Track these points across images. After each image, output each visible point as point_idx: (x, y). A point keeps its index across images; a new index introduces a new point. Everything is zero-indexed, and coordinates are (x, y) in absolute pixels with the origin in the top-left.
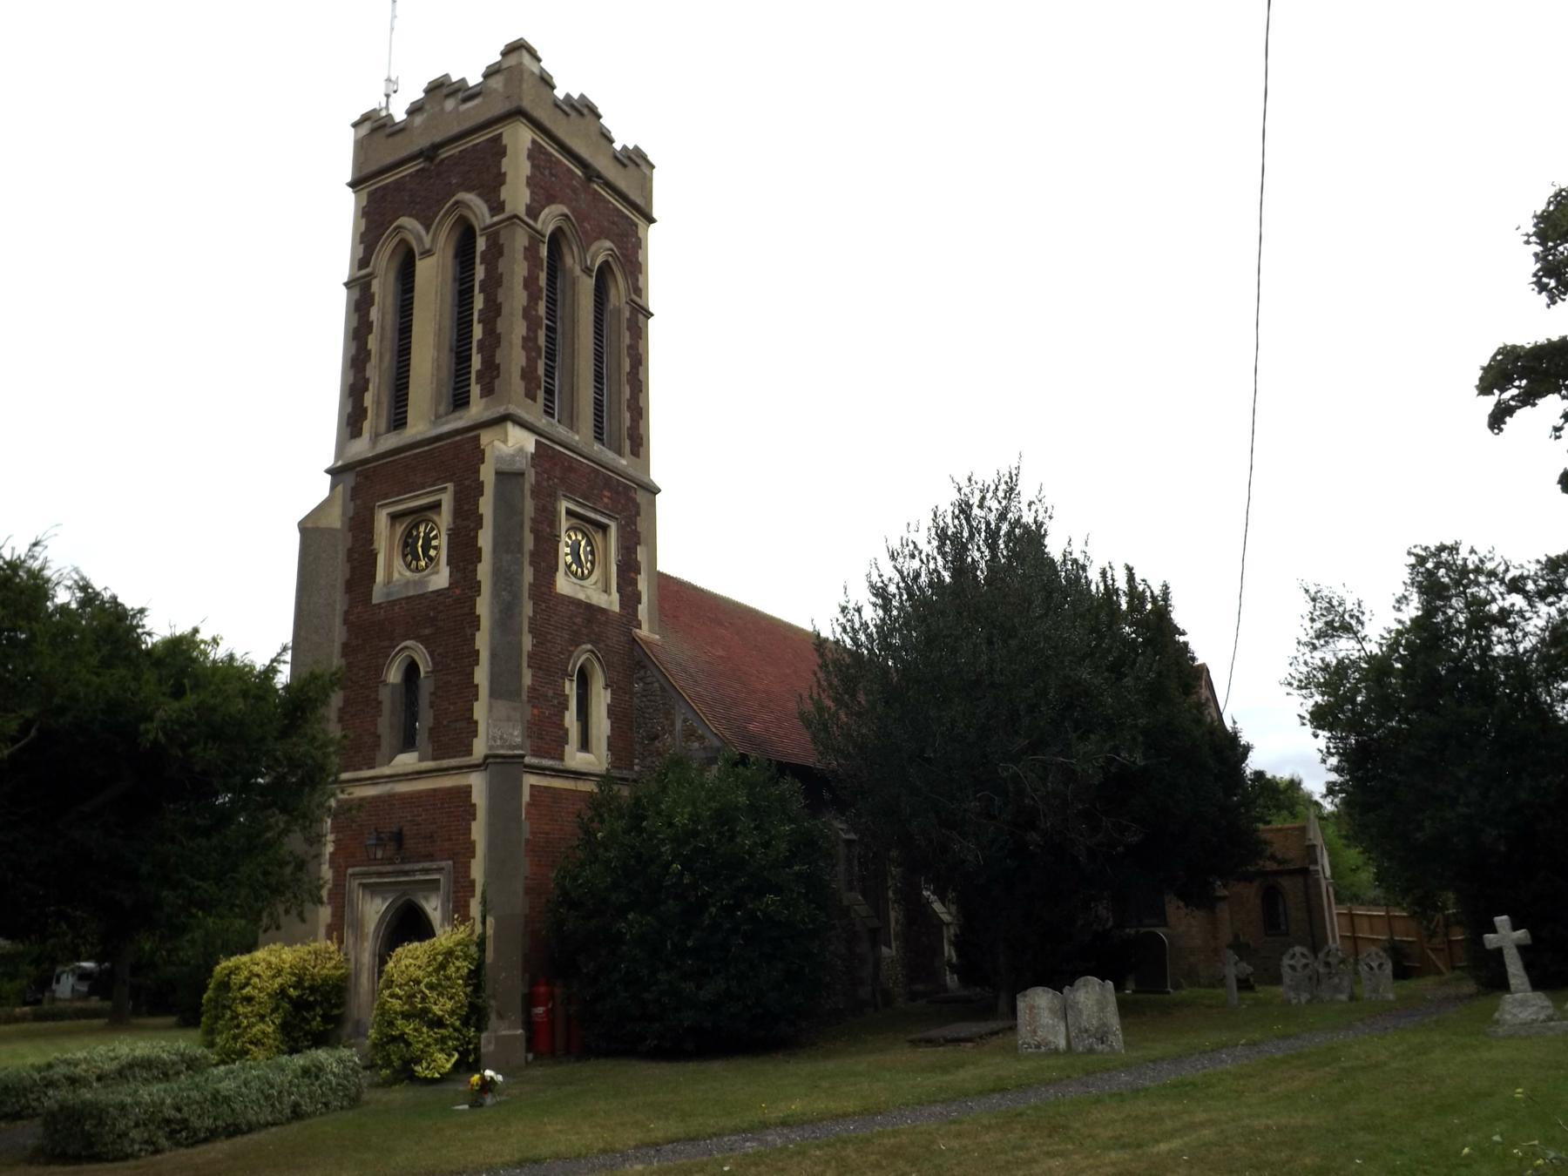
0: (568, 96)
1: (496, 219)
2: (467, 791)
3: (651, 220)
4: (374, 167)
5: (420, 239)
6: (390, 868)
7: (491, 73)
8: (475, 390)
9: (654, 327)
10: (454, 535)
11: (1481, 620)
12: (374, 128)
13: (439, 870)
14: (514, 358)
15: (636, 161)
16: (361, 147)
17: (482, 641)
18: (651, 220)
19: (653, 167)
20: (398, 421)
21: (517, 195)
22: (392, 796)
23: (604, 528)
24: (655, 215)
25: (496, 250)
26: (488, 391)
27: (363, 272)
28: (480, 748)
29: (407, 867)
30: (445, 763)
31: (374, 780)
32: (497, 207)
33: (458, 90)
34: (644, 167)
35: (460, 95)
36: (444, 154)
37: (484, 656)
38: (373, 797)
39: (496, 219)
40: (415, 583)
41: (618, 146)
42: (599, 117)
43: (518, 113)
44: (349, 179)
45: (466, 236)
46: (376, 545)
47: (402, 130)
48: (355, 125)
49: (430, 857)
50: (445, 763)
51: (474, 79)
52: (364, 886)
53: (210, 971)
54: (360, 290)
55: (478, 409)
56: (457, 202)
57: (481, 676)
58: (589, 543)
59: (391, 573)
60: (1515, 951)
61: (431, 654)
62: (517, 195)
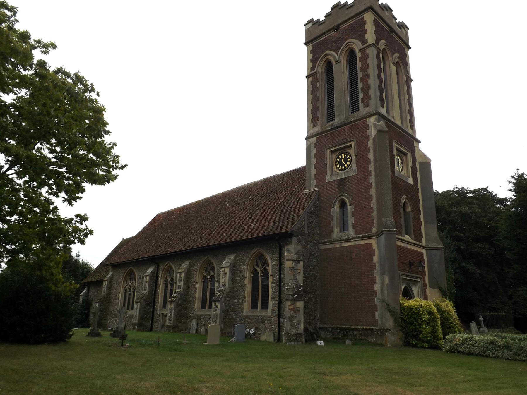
0: (382, 3)
1: (364, 46)
3: (409, 48)
4: (313, 37)
5: (334, 57)
7: (327, 16)
8: (361, 105)
9: (413, 84)
11: (448, 213)
12: (312, 24)
14: (374, 92)
15: (403, 26)
16: (308, 32)
18: (409, 48)
19: (408, 29)
20: (331, 117)
21: (370, 37)
22: (407, 248)
23: (405, 154)
24: (410, 45)
25: (365, 57)
26: (367, 105)
27: (313, 72)
29: (414, 275)
32: (364, 41)
33: (317, 22)
34: (406, 29)
35: (318, 24)
38: (403, 247)
39: (364, 46)
41: (397, 21)
42: (392, 11)
43: (371, 8)
44: (305, 42)
45: (352, 54)
47: (324, 23)
48: (305, 25)
51: (322, 18)
54: (311, 76)
55: (363, 111)
56: (326, 54)
58: (401, 160)
62: (370, 37)
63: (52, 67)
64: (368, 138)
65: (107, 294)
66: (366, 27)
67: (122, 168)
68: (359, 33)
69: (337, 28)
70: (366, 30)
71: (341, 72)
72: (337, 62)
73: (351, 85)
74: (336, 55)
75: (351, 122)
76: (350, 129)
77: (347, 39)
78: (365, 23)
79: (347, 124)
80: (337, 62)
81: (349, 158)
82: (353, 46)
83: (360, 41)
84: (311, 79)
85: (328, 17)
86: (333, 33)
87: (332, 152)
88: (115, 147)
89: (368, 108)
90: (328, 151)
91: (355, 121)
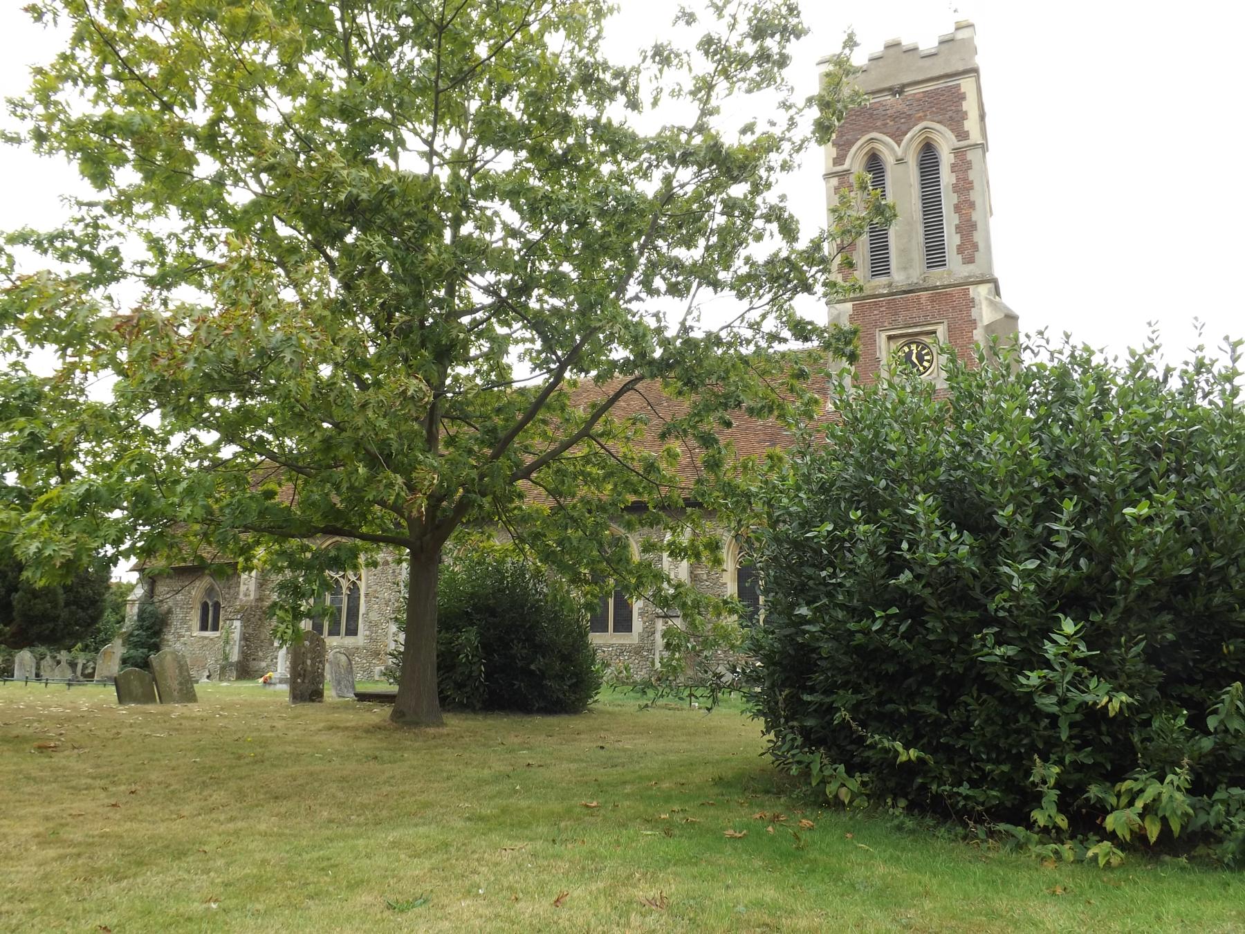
63: (141, 175)
64: (973, 323)
65: (257, 600)
66: (966, 106)
67: (39, 71)
68: (950, 113)
69: (899, 90)
70: (966, 113)
71: (903, 187)
72: (900, 161)
73: (925, 213)
74: (896, 146)
75: (936, 288)
76: (932, 300)
77: (921, 119)
78: (963, 97)
79: (926, 289)
80: (900, 161)
81: (927, 354)
82: (936, 137)
83: (952, 130)
84: (834, 181)
85: (946, 46)
86: (888, 99)
87: (890, 338)
88: (16, 145)
89: (971, 266)
90: (884, 335)
91: (945, 287)
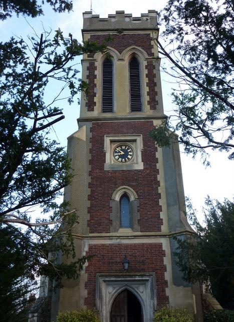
2: (160, 245)
4: (89, 29)
6: (120, 274)
10: (144, 153)
13: (149, 276)
17: (161, 190)
28: (164, 229)
30: (148, 233)
31: (110, 238)
36: (126, 33)
37: (163, 195)
40: (121, 166)
46: (105, 149)
49: (144, 270)
50: (148, 233)
52: (105, 281)
53: (195, 233)
57: (162, 202)
59: (111, 160)
60: (134, 113)
61: (137, 192)
